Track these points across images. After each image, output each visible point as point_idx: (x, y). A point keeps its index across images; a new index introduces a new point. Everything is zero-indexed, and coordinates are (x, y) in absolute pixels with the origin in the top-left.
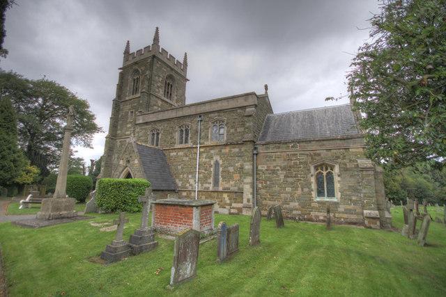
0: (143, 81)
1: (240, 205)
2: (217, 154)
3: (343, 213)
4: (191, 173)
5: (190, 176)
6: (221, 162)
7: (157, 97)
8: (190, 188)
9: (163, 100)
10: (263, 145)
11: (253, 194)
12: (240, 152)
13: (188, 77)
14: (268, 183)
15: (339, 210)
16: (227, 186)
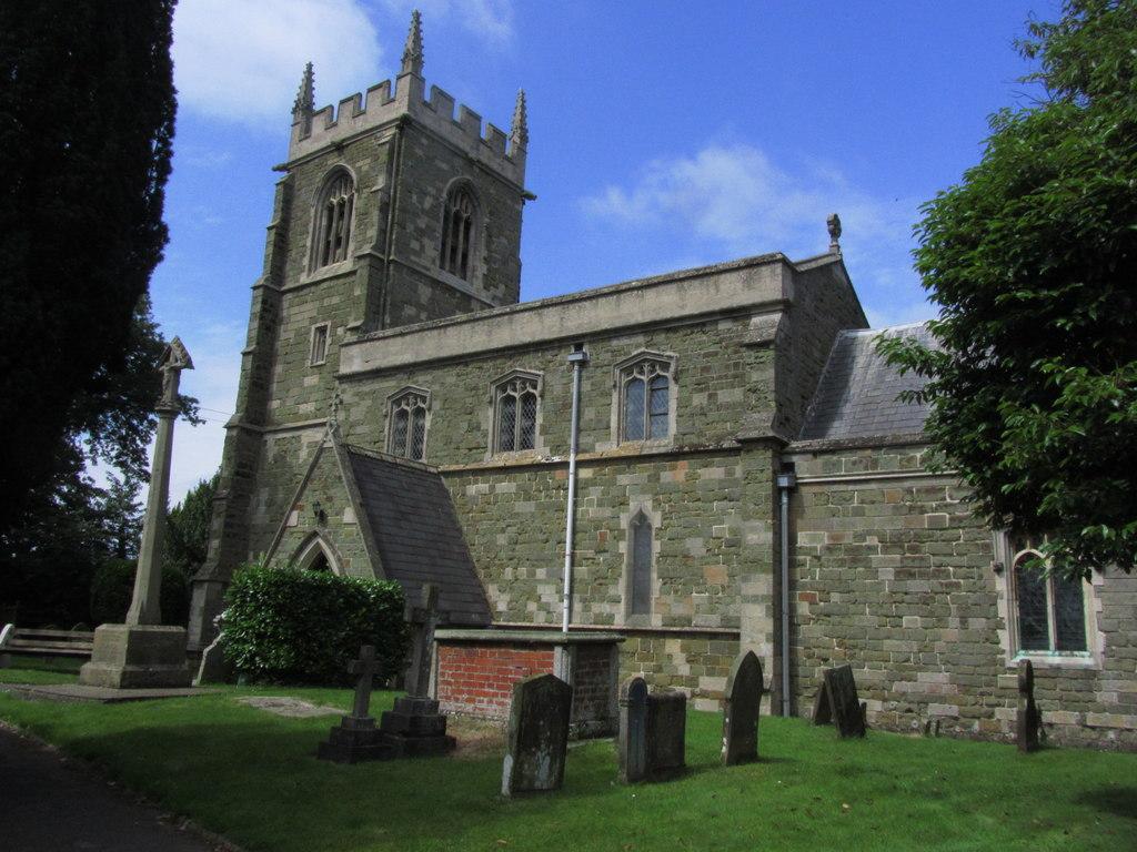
0: (364, 214)
2: (643, 492)
5: (541, 573)
6: (656, 520)
9: (435, 283)
12: (730, 478)
13: (529, 186)
14: (835, 597)
15: (1100, 697)
16: (679, 610)
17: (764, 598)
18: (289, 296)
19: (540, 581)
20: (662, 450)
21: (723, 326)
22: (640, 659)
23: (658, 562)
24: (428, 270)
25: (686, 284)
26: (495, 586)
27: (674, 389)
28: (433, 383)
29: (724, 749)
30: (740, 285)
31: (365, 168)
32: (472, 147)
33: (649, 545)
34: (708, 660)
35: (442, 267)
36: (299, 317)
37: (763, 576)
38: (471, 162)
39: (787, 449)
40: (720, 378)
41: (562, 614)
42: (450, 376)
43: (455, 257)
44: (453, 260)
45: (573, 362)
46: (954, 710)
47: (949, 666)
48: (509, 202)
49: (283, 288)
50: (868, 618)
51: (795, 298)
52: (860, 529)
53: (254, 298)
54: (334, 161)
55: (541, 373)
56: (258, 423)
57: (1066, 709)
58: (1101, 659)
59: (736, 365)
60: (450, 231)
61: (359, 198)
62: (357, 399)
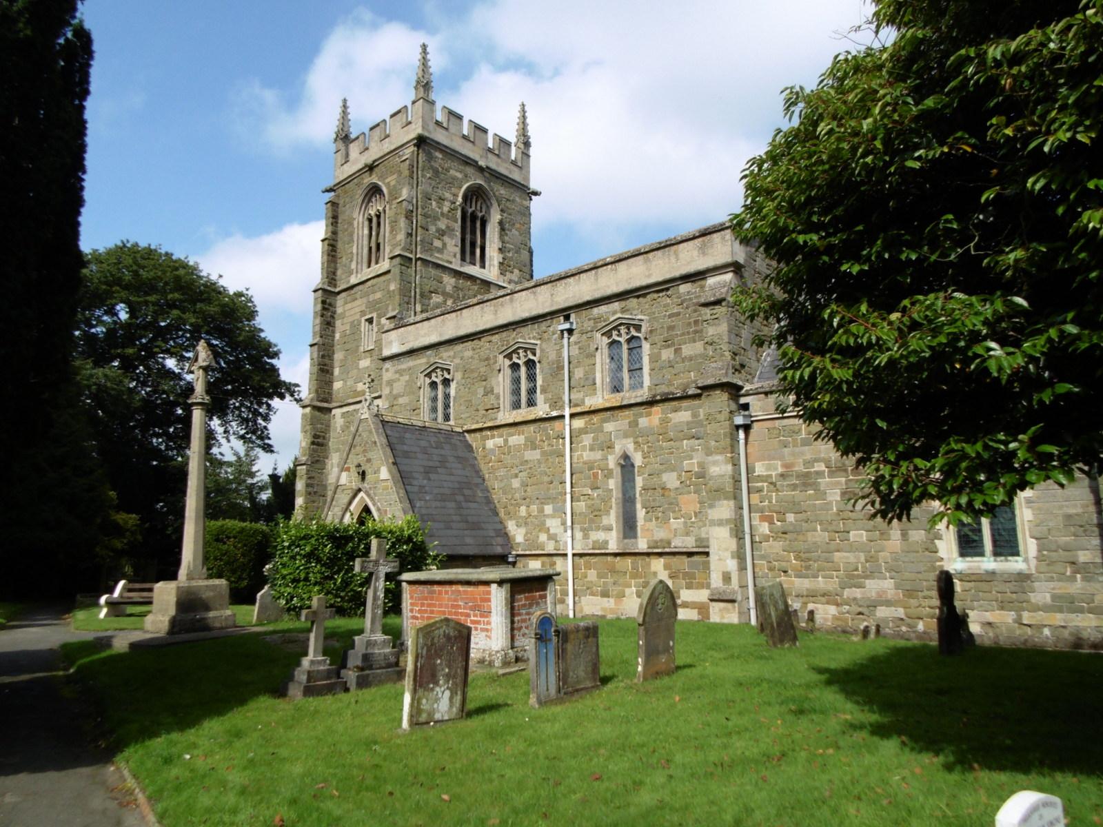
0: (394, 222)
1: (702, 595)
2: (626, 436)
3: (1046, 608)
4: (544, 501)
5: (548, 509)
6: (638, 460)
7: (438, 266)
8: (550, 548)
9: (457, 274)
10: (766, 394)
11: (740, 556)
12: (695, 422)
13: (533, 185)
14: (791, 517)
15: (1035, 598)
16: (660, 534)
17: (728, 521)
18: (343, 295)
19: (548, 516)
20: (639, 400)
21: (684, 288)
22: (631, 578)
23: (641, 494)
24: (451, 263)
25: (651, 255)
26: (514, 522)
27: (646, 347)
28: (454, 358)
29: (640, 668)
30: (695, 253)
31: (393, 183)
32: (481, 157)
33: (634, 480)
34: (686, 575)
35: (463, 259)
36: (352, 312)
37: (725, 502)
38: (481, 170)
39: (743, 392)
40: (683, 334)
41: (566, 543)
42: (466, 350)
43: (472, 248)
44: (473, 253)
45: (562, 331)
46: (901, 612)
47: (894, 573)
48: (517, 199)
49: (337, 290)
50: (819, 535)
51: (746, 260)
52: (808, 457)
53: (316, 299)
54: (369, 180)
55: (538, 342)
56: (327, 401)
57: (1002, 608)
58: (1033, 563)
59: (696, 322)
60: (468, 230)
61: (390, 209)
62: (397, 376)
